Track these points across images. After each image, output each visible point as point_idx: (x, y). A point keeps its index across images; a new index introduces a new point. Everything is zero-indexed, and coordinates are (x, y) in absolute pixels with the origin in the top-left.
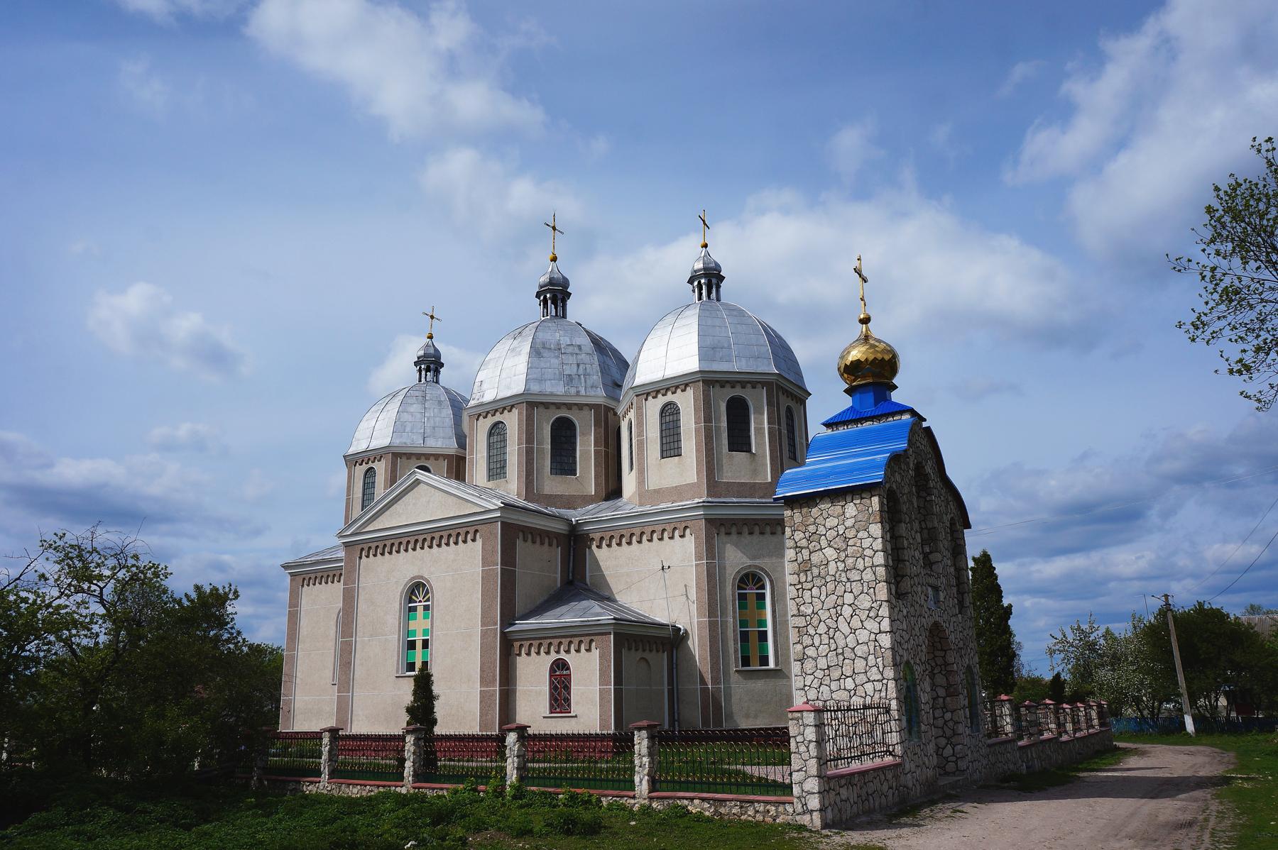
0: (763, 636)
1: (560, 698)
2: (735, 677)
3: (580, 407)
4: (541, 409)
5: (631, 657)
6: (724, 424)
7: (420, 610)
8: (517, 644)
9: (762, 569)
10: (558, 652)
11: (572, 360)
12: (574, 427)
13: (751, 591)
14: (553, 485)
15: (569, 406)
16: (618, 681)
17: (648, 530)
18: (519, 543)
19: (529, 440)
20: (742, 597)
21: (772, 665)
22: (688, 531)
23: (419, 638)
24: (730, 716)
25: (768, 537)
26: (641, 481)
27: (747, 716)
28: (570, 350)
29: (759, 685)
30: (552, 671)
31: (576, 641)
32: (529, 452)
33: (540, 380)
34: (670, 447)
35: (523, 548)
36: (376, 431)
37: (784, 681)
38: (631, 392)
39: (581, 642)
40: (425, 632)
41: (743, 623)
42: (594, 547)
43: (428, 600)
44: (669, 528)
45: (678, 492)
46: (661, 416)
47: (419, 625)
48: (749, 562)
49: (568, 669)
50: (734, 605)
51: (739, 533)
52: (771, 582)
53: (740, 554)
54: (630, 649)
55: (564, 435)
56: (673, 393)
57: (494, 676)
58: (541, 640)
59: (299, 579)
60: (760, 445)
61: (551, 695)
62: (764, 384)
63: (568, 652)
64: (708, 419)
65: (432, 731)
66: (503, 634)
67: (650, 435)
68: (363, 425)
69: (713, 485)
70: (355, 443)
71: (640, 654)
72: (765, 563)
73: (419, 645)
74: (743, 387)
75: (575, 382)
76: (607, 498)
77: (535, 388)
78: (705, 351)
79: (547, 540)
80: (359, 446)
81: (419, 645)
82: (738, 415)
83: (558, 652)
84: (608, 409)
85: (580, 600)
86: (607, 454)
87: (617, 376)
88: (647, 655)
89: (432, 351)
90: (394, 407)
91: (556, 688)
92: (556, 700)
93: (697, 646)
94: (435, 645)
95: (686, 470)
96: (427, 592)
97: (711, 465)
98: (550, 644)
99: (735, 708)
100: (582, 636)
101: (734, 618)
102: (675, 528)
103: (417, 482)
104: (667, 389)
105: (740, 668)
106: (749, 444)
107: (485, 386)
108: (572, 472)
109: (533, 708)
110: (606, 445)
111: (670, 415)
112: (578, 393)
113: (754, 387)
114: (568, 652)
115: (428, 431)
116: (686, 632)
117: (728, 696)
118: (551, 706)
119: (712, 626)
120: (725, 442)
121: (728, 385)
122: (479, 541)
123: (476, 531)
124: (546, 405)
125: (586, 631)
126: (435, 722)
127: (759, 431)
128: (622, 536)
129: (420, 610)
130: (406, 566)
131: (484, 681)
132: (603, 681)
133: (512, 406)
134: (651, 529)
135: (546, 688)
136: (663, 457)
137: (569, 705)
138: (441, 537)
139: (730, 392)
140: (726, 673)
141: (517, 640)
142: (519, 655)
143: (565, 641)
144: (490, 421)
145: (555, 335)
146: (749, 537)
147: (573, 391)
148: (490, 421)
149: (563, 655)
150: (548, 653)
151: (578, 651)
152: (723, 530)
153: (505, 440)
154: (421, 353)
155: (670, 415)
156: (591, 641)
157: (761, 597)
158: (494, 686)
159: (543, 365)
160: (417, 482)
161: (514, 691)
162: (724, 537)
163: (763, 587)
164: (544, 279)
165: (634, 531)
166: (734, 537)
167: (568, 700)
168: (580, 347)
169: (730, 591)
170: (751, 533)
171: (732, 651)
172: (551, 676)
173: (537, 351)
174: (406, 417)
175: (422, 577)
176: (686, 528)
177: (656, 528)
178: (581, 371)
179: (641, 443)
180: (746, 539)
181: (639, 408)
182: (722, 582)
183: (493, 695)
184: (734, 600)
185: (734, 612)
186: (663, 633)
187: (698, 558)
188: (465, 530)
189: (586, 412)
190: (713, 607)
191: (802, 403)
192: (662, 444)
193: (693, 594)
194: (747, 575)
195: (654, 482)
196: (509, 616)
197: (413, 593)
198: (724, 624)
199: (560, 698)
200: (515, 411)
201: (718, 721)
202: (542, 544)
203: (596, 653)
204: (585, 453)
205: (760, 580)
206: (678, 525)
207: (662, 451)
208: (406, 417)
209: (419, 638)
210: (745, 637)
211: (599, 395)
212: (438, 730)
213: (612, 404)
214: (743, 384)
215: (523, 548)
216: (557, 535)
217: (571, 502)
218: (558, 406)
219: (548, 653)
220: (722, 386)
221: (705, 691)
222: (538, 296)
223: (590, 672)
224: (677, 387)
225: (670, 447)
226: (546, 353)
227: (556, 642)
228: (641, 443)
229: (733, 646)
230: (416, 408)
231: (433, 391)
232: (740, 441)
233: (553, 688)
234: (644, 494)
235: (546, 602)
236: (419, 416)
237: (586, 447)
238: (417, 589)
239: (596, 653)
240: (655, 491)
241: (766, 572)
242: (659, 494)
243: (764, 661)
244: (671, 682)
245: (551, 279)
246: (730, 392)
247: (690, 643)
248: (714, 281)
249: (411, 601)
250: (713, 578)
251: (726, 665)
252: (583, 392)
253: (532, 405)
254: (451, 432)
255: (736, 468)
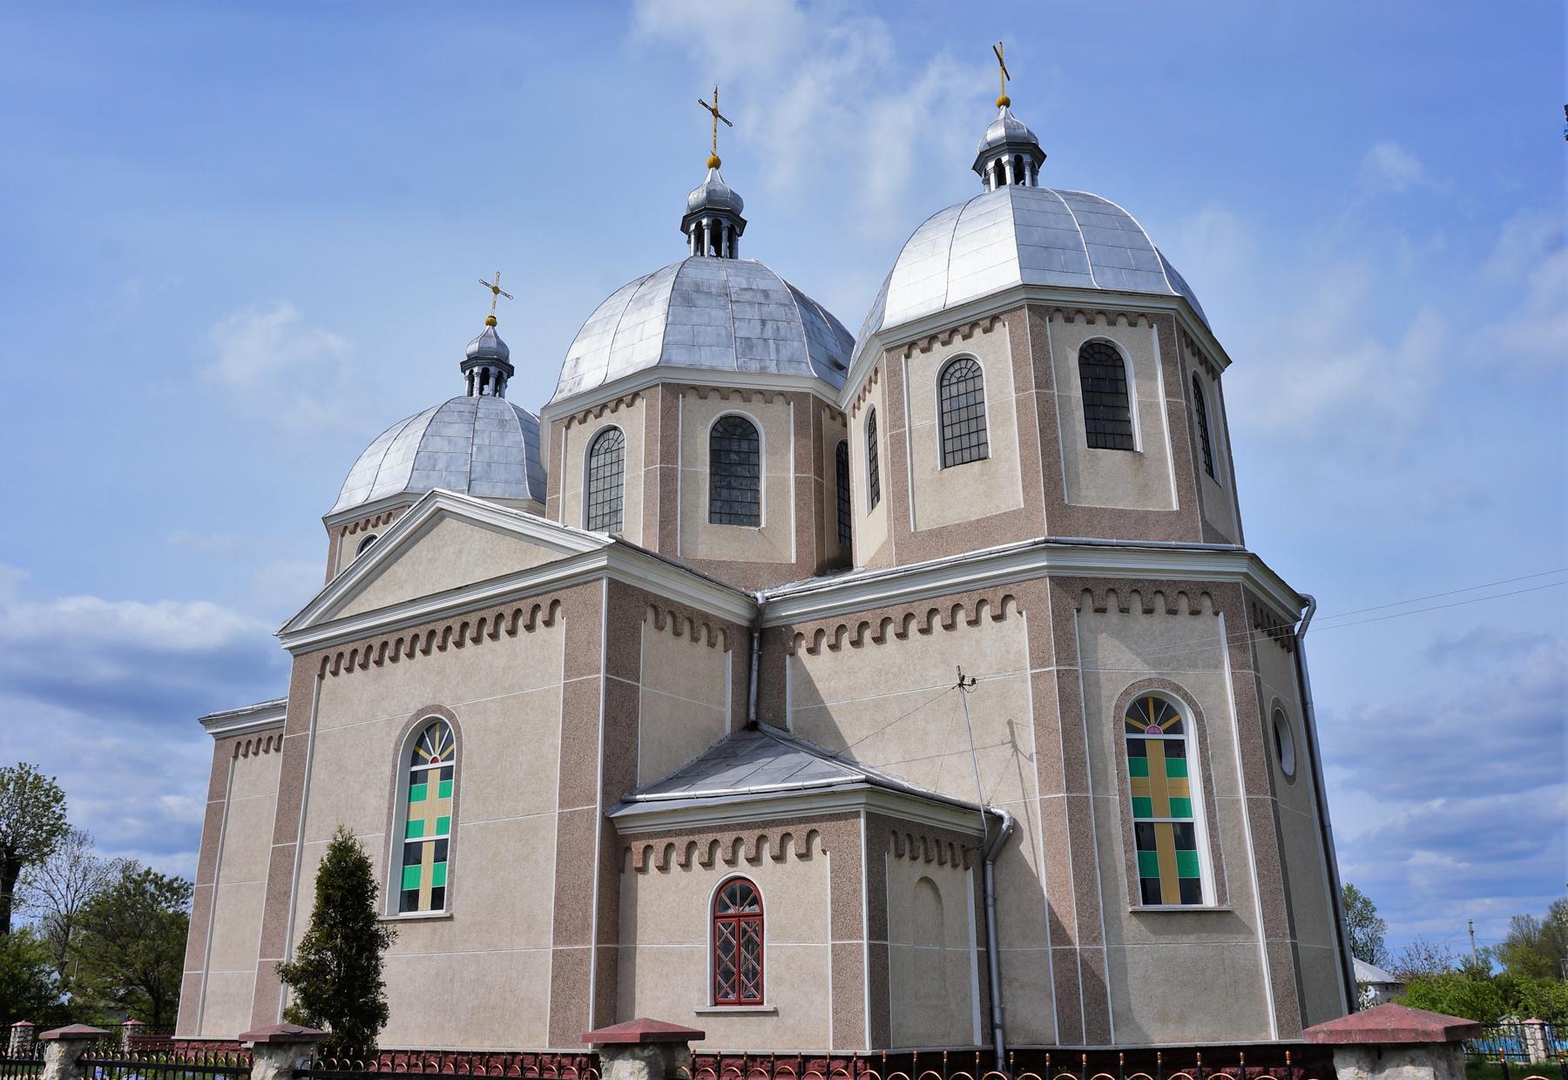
0: (1185, 837)
1: (737, 970)
2: (1132, 928)
3: (767, 396)
4: (692, 399)
5: (904, 873)
6: (1077, 393)
7: (434, 778)
8: (638, 846)
9: (1178, 689)
10: (731, 862)
11: (751, 313)
12: (756, 431)
13: (1154, 737)
14: (714, 544)
15: (745, 395)
16: (878, 929)
17: (921, 610)
18: (647, 629)
19: (668, 454)
20: (1137, 749)
21: (1209, 899)
22: (1012, 607)
23: (428, 837)
24: (1126, 1018)
25: (1184, 619)
26: (900, 515)
27: (1163, 1018)
28: (748, 296)
29: (1185, 946)
30: (718, 904)
31: (775, 834)
32: (667, 478)
33: (692, 346)
34: (962, 439)
35: (653, 642)
36: (382, 472)
37: (1241, 938)
38: (877, 344)
39: (786, 837)
40: (442, 825)
41: (1141, 806)
42: (802, 652)
43: (450, 757)
44: (968, 602)
45: (983, 529)
46: (941, 386)
47: (430, 808)
48: (1151, 673)
49: (756, 901)
50: (1119, 764)
51: (1124, 610)
52: (1199, 716)
53: (1128, 656)
54: (900, 856)
55: (734, 448)
56: (965, 338)
57: (586, 918)
58: (692, 838)
59: (231, 744)
60: (1152, 436)
61: (717, 962)
62: (1151, 318)
63: (755, 860)
64: (1043, 382)
65: (368, 1039)
66: (609, 823)
67: (917, 424)
68: (364, 462)
69: (1058, 508)
70: (345, 495)
71: (920, 869)
72: (1188, 679)
73: (428, 853)
74: (1112, 323)
75: (758, 350)
76: (822, 572)
77: (680, 358)
78: (1029, 252)
79: (704, 633)
80: (355, 494)
81: (428, 853)
82: (1103, 373)
83: (731, 862)
84: (820, 404)
85: (777, 756)
86: (819, 488)
87: (837, 352)
88: (933, 871)
89: (493, 344)
90: (418, 428)
91: (727, 947)
92: (727, 974)
93: (1041, 854)
94: (460, 855)
95: (1002, 484)
96: (449, 741)
97: (1053, 475)
98: (714, 844)
99: (1137, 1001)
100: (790, 824)
101: (1122, 793)
102: (982, 601)
103: (440, 515)
104: (953, 331)
105: (1141, 907)
106: (1130, 436)
107: (583, 367)
108: (754, 519)
109: (672, 984)
110: (819, 470)
111: (959, 379)
112: (763, 371)
113: (1133, 324)
114: (755, 860)
115: (478, 469)
116: (1015, 825)
117: (1120, 969)
118: (716, 987)
119: (1077, 810)
120: (1081, 428)
121: (1080, 319)
122: (561, 624)
123: (556, 603)
124: (701, 392)
125: (798, 810)
126: (377, 1015)
127: (1149, 408)
128: (863, 625)
129: (434, 778)
130: (409, 687)
131: (562, 930)
132: (842, 925)
133: (636, 395)
134: (927, 606)
135: (705, 947)
136: (945, 465)
137: (759, 987)
138: (483, 621)
139: (1084, 333)
140: (1112, 919)
141: (637, 837)
142: (643, 870)
143: (750, 837)
144: (593, 426)
145: (715, 272)
146: (1143, 618)
147: (754, 366)
148: (593, 426)
149: (743, 870)
150: (708, 864)
151: (779, 858)
152: (1088, 601)
153: (619, 461)
154: (474, 348)
155: (959, 379)
156: (812, 833)
157: (1176, 750)
158: (586, 941)
159: (695, 319)
160: (440, 515)
161: (631, 955)
162: (1091, 618)
163: (1178, 728)
164: (696, 196)
165: (889, 613)
166: (1113, 617)
167: (756, 975)
168: (766, 293)
169: (1111, 735)
170: (1148, 611)
171: (1122, 867)
172: (715, 918)
173: (684, 297)
174: (437, 444)
175: (439, 708)
176: (1007, 598)
177: (937, 603)
178: (769, 333)
179: (898, 444)
180: (1139, 622)
181: (895, 374)
182: (1094, 714)
183: (582, 961)
184: (1119, 754)
185: (1122, 780)
186: (969, 826)
187: (1038, 659)
188: (531, 602)
189: (778, 406)
190: (1075, 768)
191: (1215, 374)
192: (943, 440)
193: (1028, 740)
194: (1142, 703)
195: (928, 514)
196: (620, 784)
197: (420, 742)
198: (1102, 806)
199: (737, 970)
200: (641, 404)
201: (1101, 1030)
202: (695, 639)
203: (822, 864)
204: (778, 486)
205: (1171, 712)
206: (988, 595)
207: (944, 454)
208: (437, 444)
209: (428, 837)
210: (1145, 837)
211: (805, 377)
212: (386, 1039)
213: (828, 395)
214: (1112, 318)
215: (653, 642)
216: (727, 627)
217: (752, 572)
218: (724, 393)
219: (708, 864)
220: (1069, 320)
221: (1064, 958)
222: (685, 228)
223: (809, 905)
224: (974, 325)
225: (962, 439)
226: (701, 300)
227: (727, 838)
228: (898, 444)
229: (1122, 855)
230: (457, 429)
231: (488, 405)
232: (1108, 424)
233: (721, 947)
234: (904, 537)
235: (702, 761)
236: (462, 442)
237: (781, 473)
238: (428, 733)
239: (822, 864)
240: (931, 532)
241: (1185, 696)
242: (940, 537)
243: (1191, 890)
244: (984, 938)
245: (710, 193)
246: (1084, 333)
247: (1025, 848)
248: (1027, 158)
249: (416, 759)
250: (1071, 699)
251: (1111, 898)
252: (773, 368)
253: (674, 391)
254: (521, 472)
255: (1103, 480)
